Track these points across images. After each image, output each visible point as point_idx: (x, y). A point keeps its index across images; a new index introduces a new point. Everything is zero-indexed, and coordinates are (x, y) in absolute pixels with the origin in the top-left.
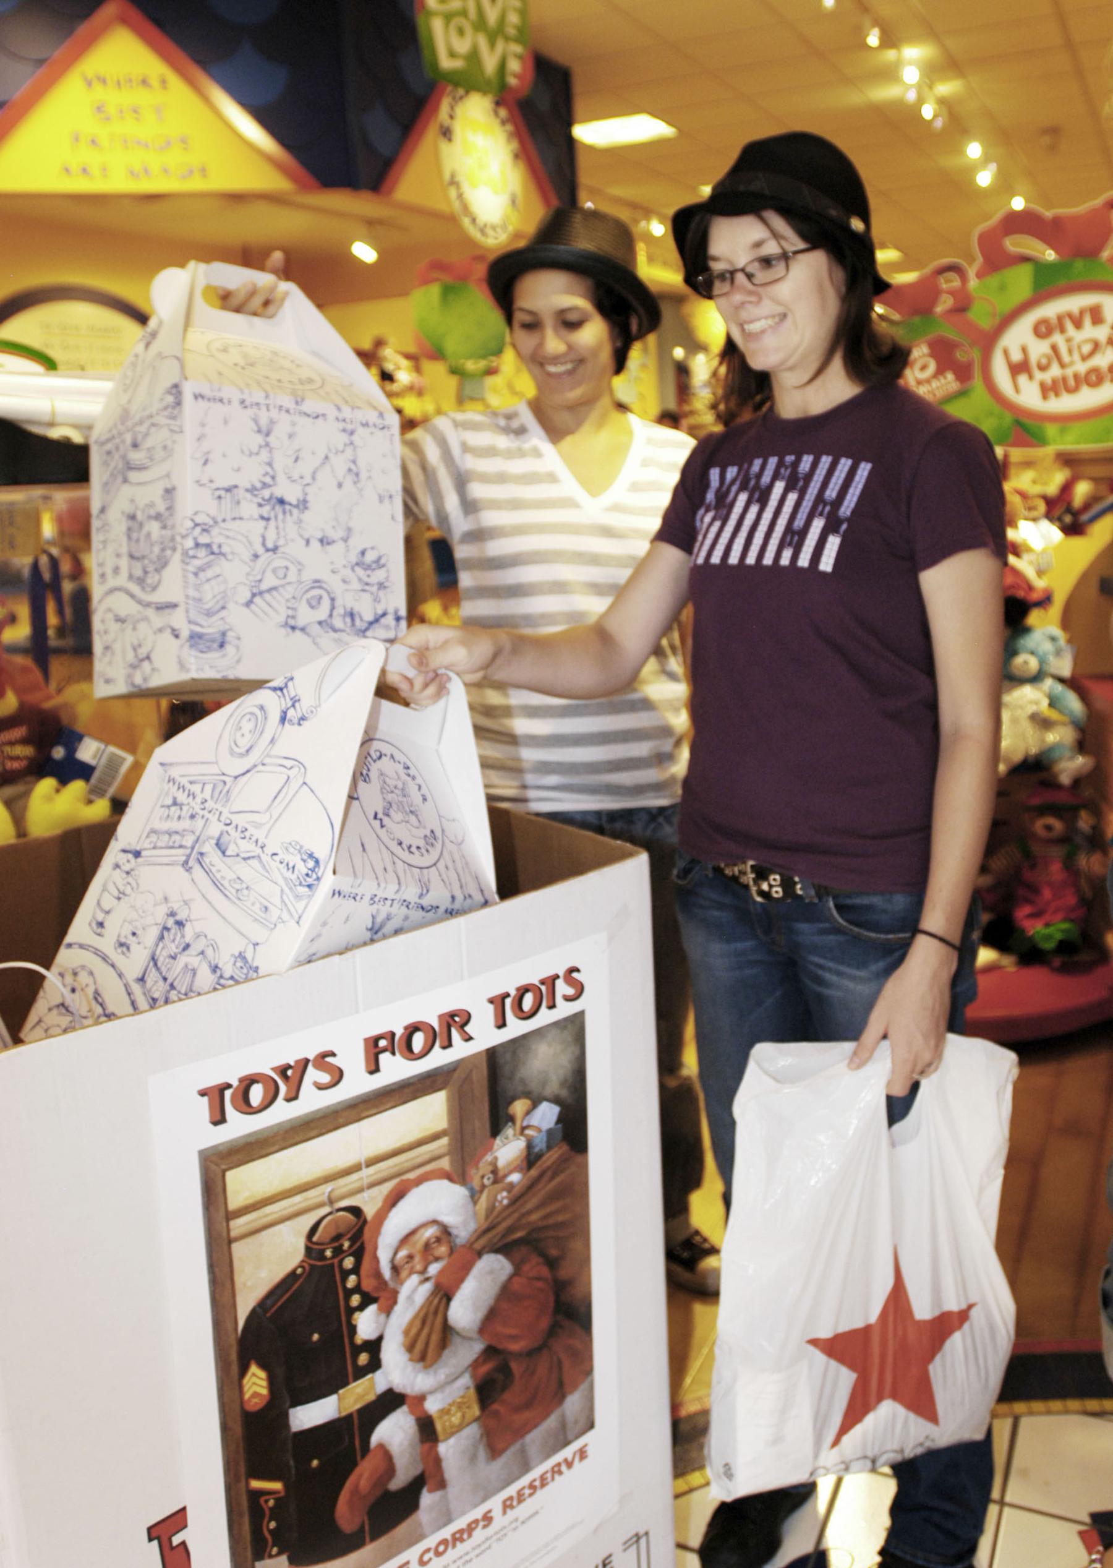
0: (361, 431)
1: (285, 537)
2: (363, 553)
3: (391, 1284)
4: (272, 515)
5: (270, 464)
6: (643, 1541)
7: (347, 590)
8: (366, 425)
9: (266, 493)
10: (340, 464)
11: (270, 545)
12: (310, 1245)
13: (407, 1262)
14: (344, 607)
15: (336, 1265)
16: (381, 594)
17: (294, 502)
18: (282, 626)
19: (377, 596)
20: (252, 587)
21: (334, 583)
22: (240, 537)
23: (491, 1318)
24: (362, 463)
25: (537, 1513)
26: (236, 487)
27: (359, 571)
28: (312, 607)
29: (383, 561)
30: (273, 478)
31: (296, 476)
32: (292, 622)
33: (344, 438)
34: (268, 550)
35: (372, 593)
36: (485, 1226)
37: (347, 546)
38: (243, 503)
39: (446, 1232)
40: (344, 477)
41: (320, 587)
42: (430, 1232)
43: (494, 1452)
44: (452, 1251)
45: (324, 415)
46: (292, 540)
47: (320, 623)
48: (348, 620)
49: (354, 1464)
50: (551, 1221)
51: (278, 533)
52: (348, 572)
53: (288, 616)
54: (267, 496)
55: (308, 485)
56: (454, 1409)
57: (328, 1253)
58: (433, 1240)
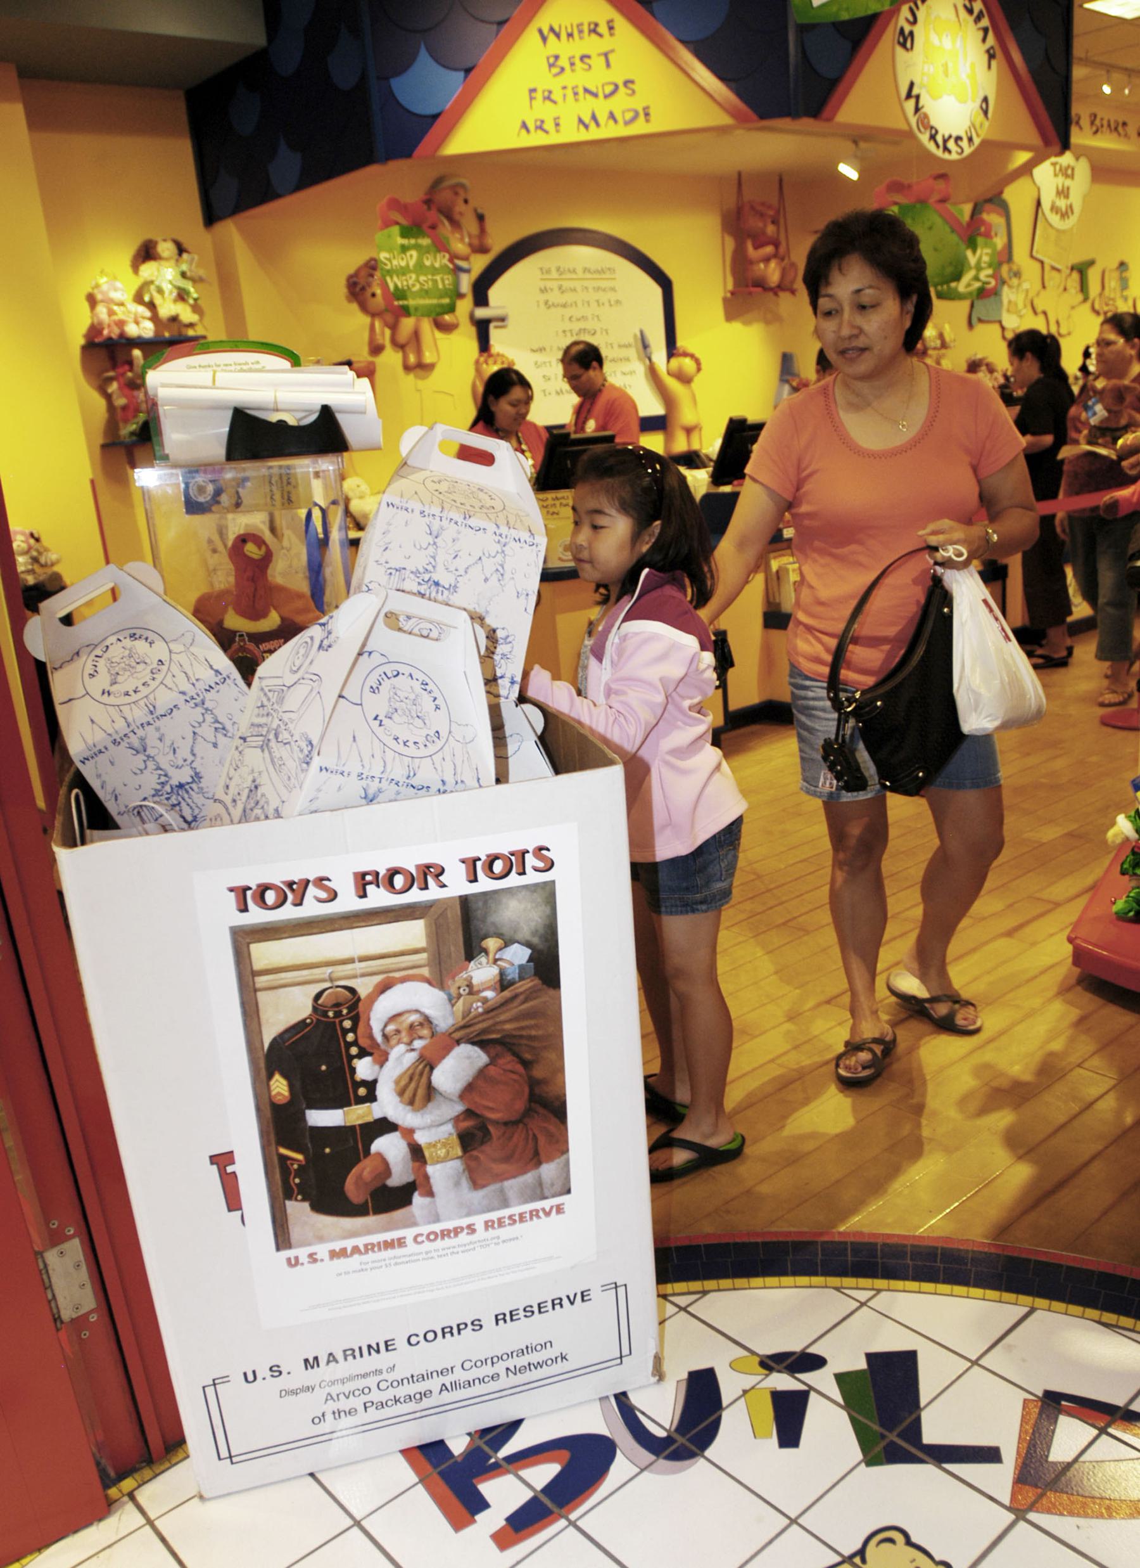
23: (469, 1090)
29: (509, 639)
39: (427, 1021)
57: (331, 1014)
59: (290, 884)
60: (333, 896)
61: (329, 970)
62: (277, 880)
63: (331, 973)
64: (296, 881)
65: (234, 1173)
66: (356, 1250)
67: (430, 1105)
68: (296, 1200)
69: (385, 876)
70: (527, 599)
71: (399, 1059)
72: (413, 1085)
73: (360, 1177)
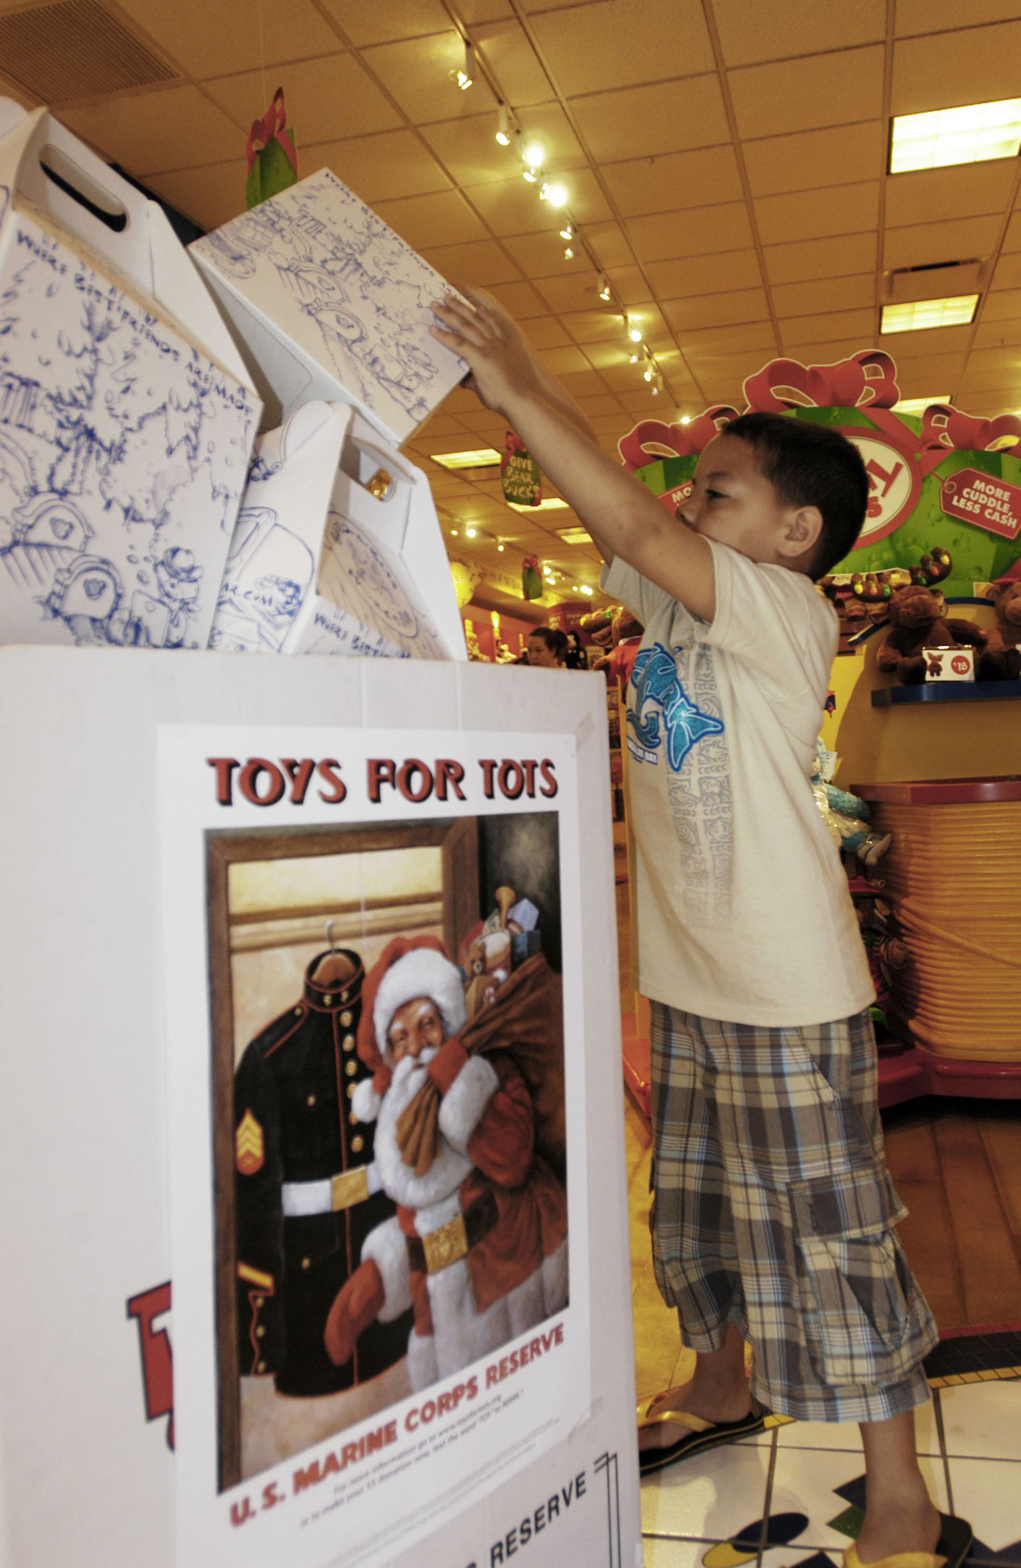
0: (213, 395)
1: (81, 483)
2: (175, 552)
3: (386, 1060)
4: (73, 446)
5: (91, 378)
6: (612, 1464)
7: (139, 592)
8: (222, 392)
9: (75, 414)
10: (179, 424)
11: (58, 484)
12: (309, 984)
13: (402, 1039)
14: (131, 613)
15: (334, 1017)
16: (182, 616)
17: (107, 444)
18: (41, 603)
19: (177, 614)
20: (17, 530)
21: (127, 575)
22: (20, 454)
23: (479, 1132)
24: (205, 436)
25: (516, 1396)
26: (36, 384)
27: (163, 574)
28: (89, 595)
29: (195, 574)
30: (90, 398)
31: (119, 411)
32: (56, 603)
33: (192, 395)
34: (53, 490)
35: (171, 611)
36: (473, 1022)
37: (157, 535)
38: (39, 412)
39: (438, 1015)
40: (178, 444)
41: (108, 573)
42: (423, 1010)
43: (481, 1305)
44: (444, 1038)
45: (176, 353)
46: (89, 492)
47: (94, 620)
48: (131, 632)
49: (343, 1278)
50: (531, 1040)
51: (73, 474)
52: (148, 568)
53: (53, 593)
54: (74, 418)
55: (130, 430)
56: (442, 1236)
57: (327, 1000)
58: (426, 1020)
59: (291, 765)
60: (341, 796)
61: (328, 920)
62: (274, 756)
63: (331, 927)
64: (299, 761)
65: (164, 1332)
66: (332, 1464)
67: (437, 1163)
68: (257, 1373)
69: (402, 771)
70: (226, 504)
71: (404, 1082)
72: (417, 1129)
73: (345, 1310)
